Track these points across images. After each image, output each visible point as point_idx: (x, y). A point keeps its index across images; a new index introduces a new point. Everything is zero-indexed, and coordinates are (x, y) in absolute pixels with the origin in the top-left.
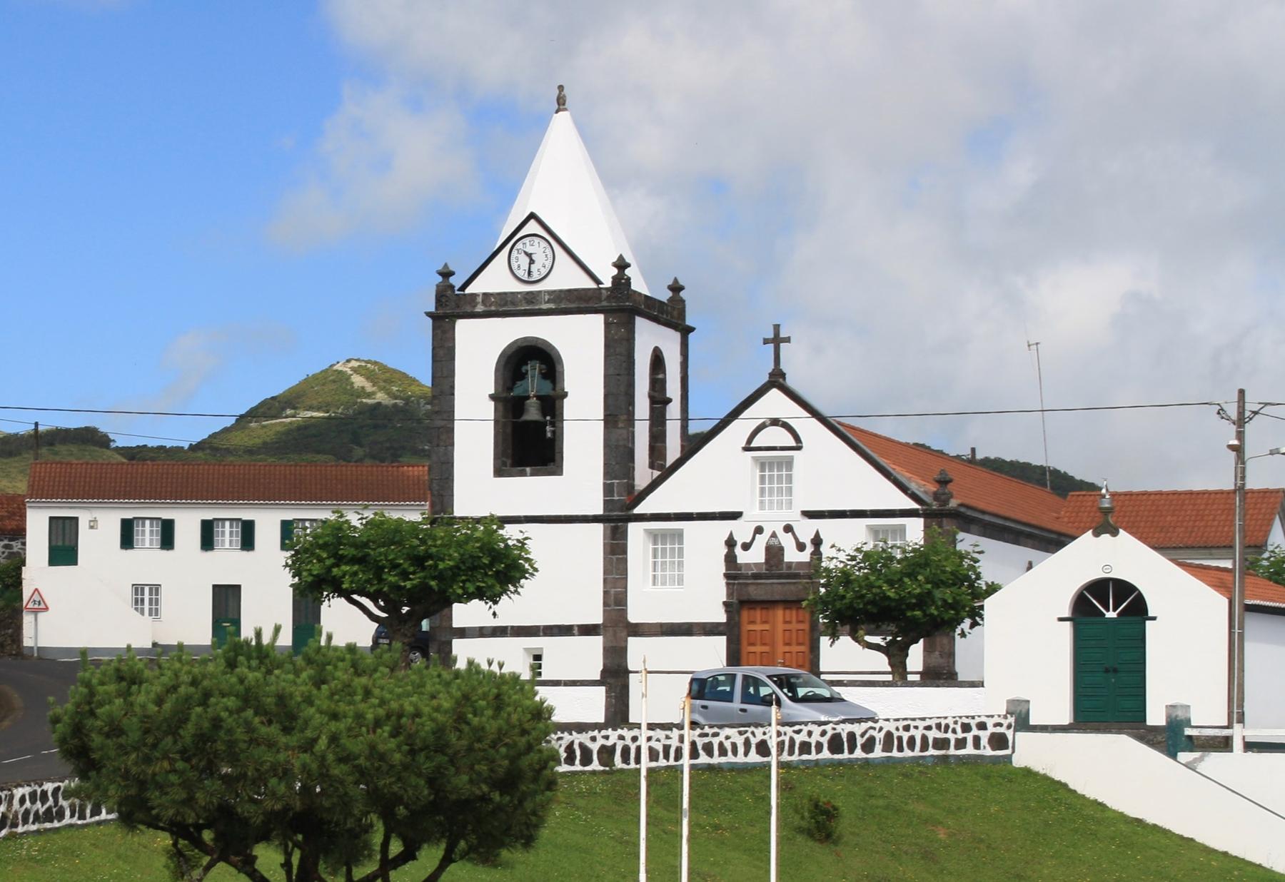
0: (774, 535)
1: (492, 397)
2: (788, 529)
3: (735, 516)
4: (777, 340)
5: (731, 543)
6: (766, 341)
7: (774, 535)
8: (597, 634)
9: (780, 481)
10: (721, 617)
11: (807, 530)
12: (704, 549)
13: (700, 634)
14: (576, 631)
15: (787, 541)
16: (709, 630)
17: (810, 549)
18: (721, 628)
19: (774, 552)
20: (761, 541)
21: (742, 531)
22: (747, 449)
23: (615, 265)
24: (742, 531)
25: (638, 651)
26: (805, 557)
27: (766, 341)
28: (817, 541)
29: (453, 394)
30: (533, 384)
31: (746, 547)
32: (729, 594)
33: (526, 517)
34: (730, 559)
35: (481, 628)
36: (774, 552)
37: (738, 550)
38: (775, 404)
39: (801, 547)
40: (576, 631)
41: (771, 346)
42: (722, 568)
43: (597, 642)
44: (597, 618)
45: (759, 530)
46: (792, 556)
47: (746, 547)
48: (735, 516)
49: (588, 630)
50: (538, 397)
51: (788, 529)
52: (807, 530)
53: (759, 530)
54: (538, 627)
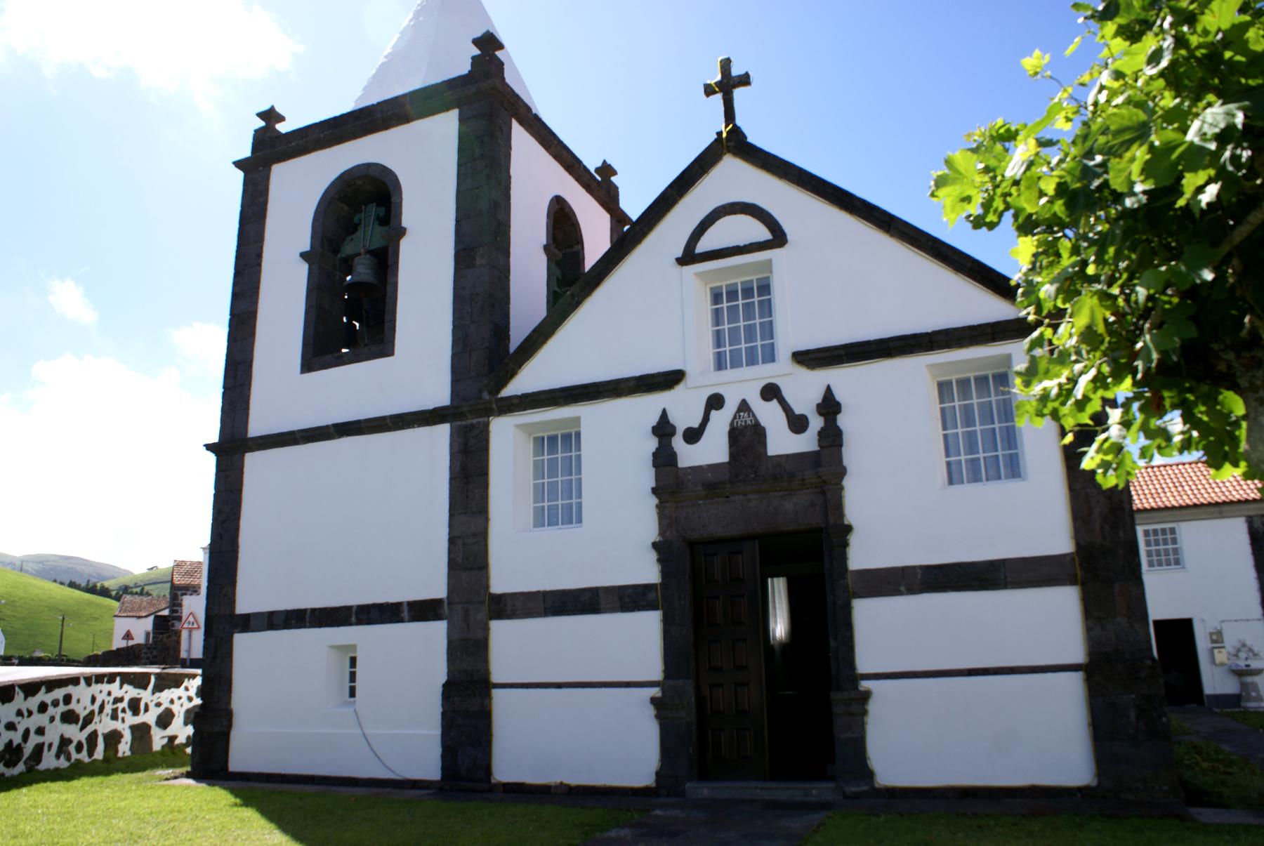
0: (744, 406)
1: (655, 545)
2: (771, 392)
3: (670, 379)
4: (728, 84)
5: (663, 429)
6: (709, 91)
7: (744, 406)
8: (437, 617)
9: (749, 314)
10: (648, 572)
11: (805, 389)
12: (616, 443)
13: (612, 610)
14: (405, 614)
15: (770, 416)
16: (629, 599)
17: (816, 423)
18: (652, 596)
19: (746, 437)
20: (721, 422)
21: (683, 406)
22: (689, 257)
23: (476, 42)
24: (683, 406)
25: (513, 647)
26: (805, 443)
27: (709, 91)
28: (830, 406)
29: (259, 265)
30: (369, 235)
31: (693, 436)
32: (662, 531)
33: (336, 426)
34: (664, 459)
35: (271, 614)
36: (746, 437)
37: (678, 443)
38: (733, 179)
39: (798, 424)
40: (405, 614)
41: (718, 99)
42: (647, 477)
43: (436, 633)
44: (435, 586)
45: (715, 402)
46: (782, 442)
47: (693, 436)
48: (670, 379)
49: (423, 611)
50: (370, 252)
51: (771, 392)
52: (805, 389)
53: (715, 402)
54: (349, 608)
